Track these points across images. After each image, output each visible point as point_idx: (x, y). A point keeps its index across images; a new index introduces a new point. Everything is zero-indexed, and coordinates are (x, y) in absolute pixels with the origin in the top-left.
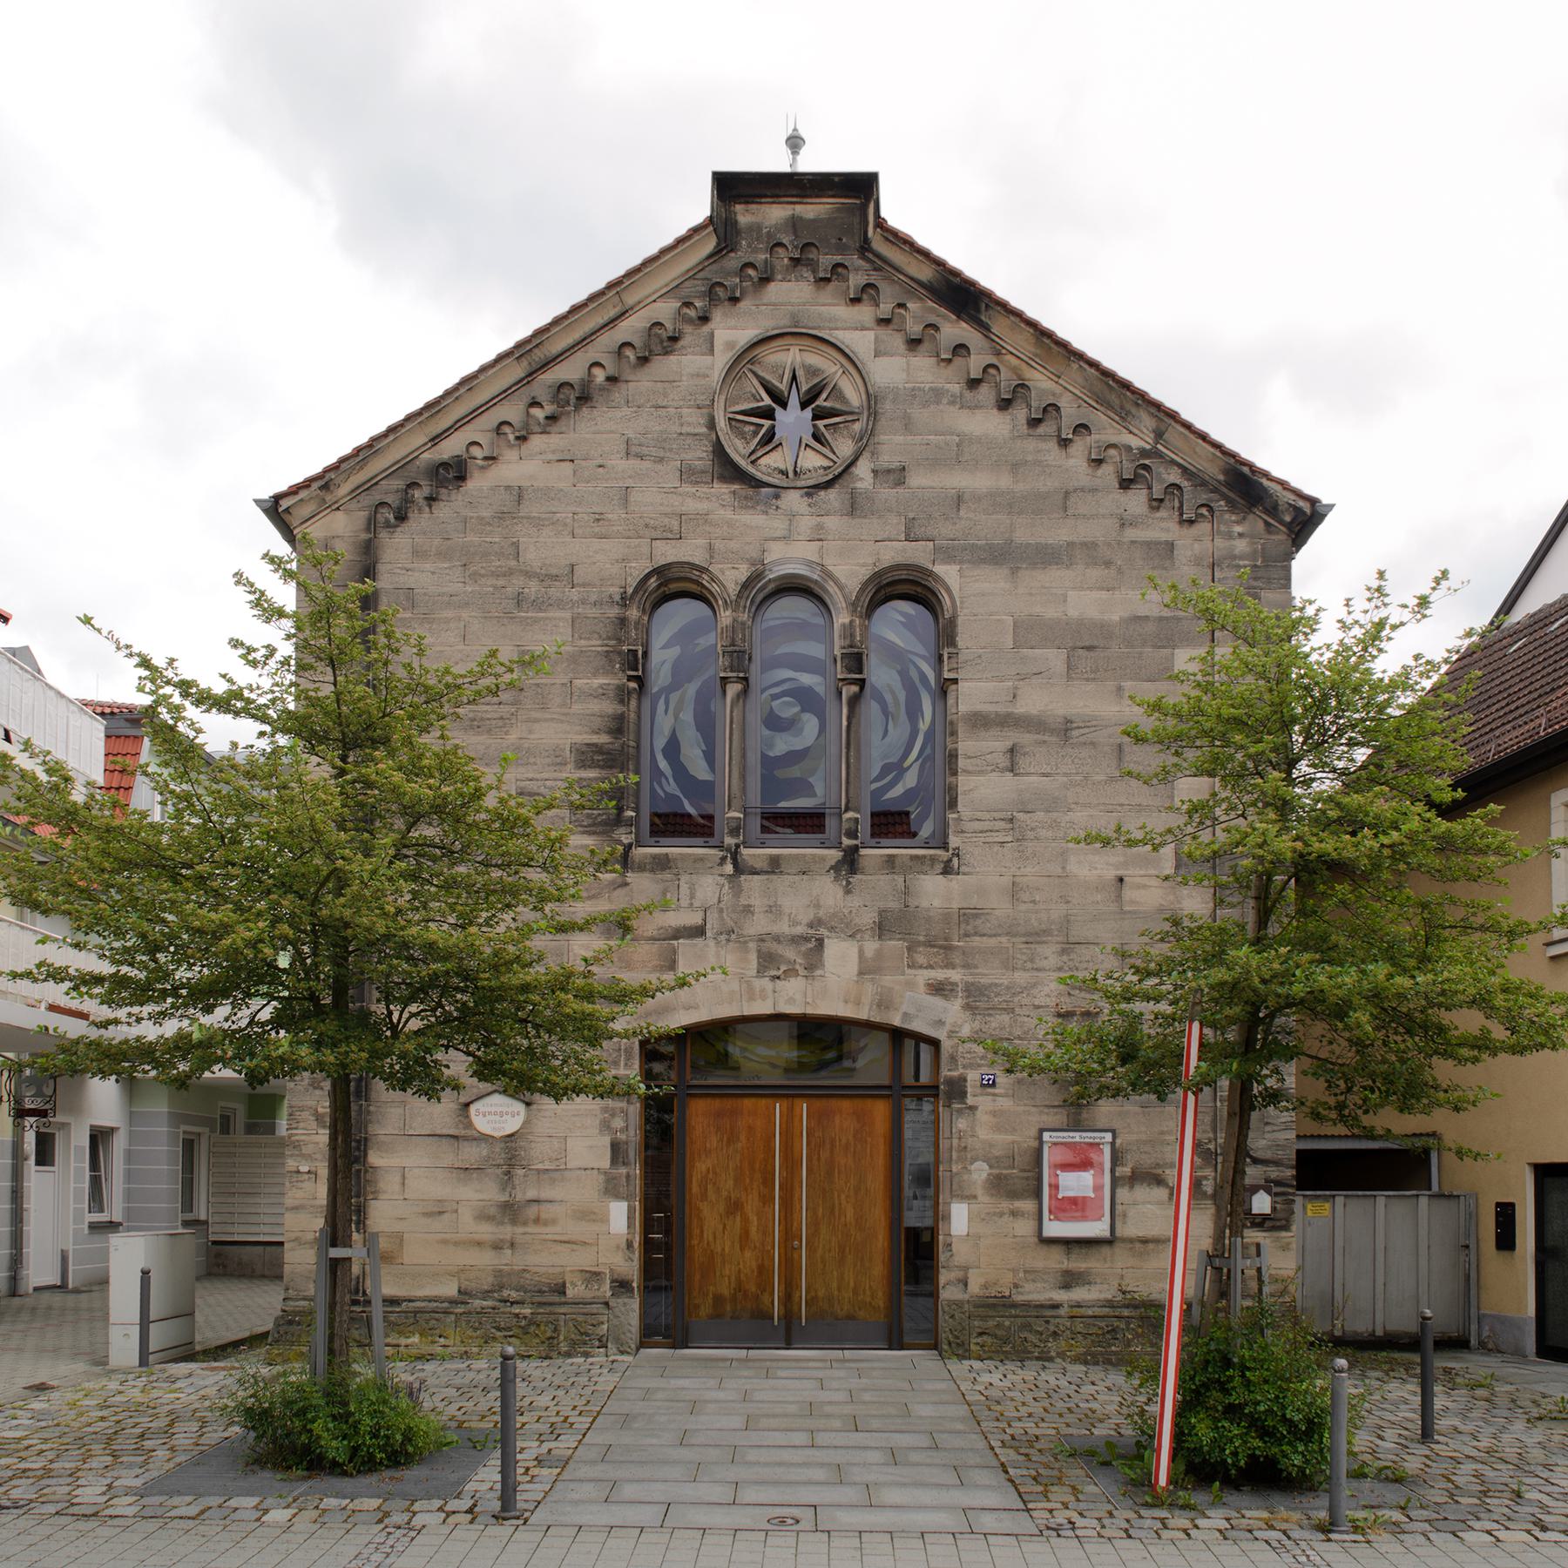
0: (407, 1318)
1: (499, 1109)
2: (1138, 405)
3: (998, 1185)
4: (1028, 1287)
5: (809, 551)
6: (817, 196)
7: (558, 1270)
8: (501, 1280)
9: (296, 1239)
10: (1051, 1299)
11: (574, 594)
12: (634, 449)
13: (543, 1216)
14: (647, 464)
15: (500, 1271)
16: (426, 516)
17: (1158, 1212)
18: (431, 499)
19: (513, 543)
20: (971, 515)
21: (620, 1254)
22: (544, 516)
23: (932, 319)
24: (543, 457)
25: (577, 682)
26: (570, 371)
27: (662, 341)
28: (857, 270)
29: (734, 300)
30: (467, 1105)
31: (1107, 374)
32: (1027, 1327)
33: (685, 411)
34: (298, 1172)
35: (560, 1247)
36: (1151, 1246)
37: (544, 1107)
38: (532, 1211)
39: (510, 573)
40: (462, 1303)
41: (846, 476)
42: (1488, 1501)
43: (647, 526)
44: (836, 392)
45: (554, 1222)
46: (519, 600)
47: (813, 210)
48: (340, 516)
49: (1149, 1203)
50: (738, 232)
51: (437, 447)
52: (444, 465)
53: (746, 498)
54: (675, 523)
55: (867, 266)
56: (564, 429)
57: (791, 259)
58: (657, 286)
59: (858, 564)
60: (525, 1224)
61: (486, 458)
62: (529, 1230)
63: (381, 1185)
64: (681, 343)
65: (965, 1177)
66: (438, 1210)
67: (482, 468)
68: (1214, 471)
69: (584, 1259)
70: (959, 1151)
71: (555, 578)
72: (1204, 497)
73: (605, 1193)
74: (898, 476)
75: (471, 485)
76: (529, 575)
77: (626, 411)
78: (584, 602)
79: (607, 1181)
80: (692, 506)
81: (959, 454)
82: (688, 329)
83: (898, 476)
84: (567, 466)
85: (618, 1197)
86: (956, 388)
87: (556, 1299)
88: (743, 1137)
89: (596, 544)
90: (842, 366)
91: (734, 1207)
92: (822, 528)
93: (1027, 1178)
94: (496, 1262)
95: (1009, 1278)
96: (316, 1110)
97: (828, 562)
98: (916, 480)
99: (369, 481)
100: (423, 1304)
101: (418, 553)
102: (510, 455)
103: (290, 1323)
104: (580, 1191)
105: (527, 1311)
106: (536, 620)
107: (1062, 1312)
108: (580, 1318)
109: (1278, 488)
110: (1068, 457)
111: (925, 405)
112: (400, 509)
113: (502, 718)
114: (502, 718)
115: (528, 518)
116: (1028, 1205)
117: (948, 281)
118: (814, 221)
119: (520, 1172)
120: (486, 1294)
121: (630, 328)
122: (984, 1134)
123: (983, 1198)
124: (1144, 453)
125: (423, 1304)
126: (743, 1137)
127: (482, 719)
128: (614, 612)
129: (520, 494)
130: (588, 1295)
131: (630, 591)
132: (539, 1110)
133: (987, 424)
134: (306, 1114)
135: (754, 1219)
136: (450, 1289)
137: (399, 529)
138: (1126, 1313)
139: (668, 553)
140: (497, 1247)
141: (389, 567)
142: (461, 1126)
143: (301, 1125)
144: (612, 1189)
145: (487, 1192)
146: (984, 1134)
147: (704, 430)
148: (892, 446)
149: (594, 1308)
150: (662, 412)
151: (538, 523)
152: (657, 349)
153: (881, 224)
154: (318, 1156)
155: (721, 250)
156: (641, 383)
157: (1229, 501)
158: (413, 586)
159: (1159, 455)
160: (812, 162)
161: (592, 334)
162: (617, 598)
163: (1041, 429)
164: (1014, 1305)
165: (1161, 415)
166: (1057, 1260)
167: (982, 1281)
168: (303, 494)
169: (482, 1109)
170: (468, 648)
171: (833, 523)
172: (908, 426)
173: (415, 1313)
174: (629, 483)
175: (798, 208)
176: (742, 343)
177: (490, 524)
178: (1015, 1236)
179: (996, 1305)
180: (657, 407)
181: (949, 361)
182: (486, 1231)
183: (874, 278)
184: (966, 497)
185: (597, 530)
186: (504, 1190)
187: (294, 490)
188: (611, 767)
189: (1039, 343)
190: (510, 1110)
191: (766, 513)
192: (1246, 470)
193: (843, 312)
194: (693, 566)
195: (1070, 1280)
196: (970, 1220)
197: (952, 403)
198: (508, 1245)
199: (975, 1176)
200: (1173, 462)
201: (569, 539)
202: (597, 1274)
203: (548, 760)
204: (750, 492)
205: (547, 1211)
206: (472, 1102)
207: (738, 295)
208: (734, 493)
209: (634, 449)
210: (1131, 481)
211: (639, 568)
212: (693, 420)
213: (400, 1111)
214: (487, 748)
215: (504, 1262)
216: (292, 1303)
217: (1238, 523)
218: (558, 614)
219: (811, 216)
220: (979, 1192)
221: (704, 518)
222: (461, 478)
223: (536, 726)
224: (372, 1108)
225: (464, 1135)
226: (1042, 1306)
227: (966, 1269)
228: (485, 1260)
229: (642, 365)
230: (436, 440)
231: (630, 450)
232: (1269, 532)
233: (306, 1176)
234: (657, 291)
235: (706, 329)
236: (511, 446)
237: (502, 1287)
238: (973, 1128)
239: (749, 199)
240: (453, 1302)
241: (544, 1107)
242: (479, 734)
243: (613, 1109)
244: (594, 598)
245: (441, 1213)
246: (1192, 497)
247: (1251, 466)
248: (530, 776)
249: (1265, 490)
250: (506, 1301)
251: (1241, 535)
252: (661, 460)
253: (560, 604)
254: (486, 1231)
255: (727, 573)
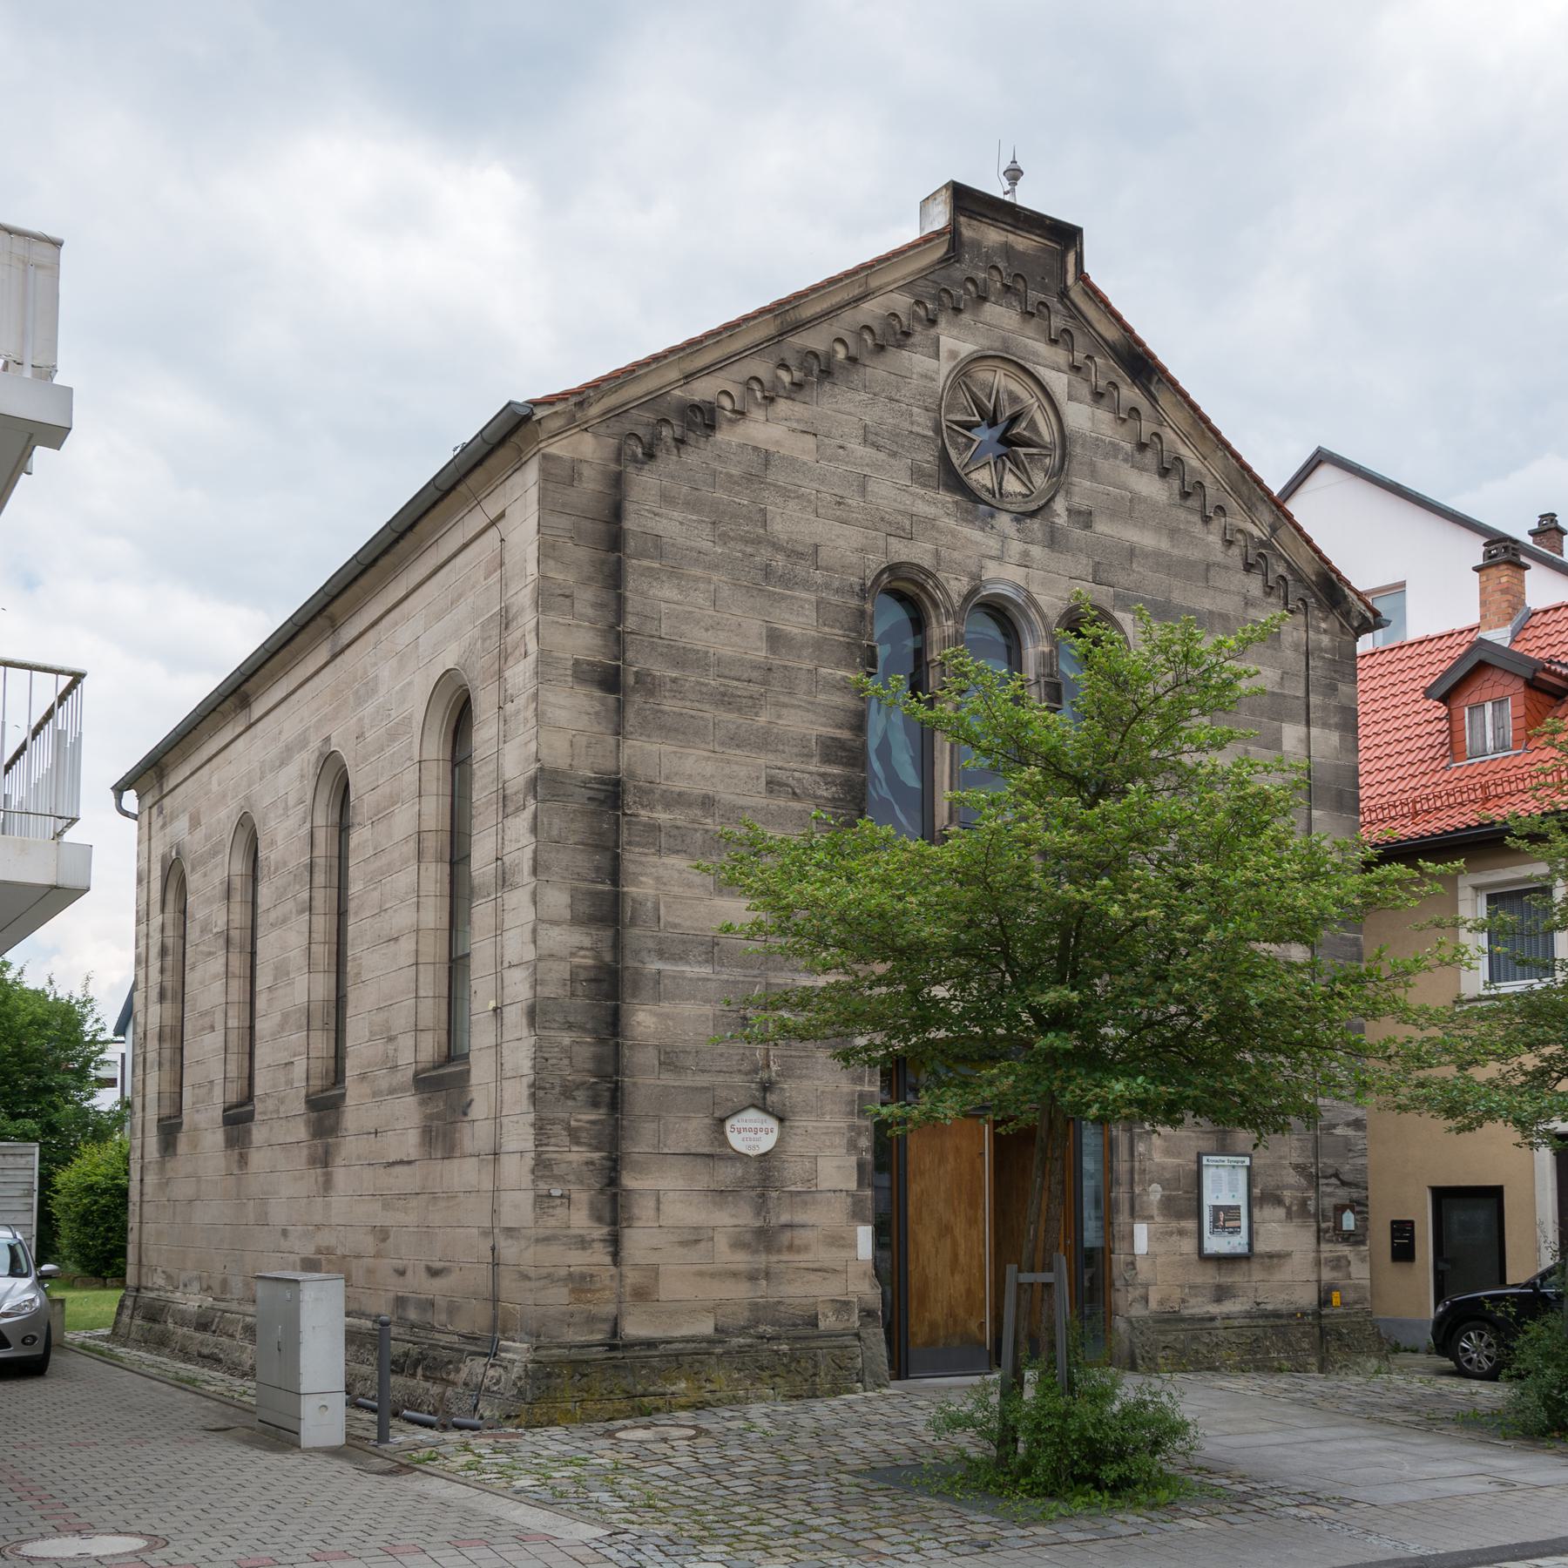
0: (668, 1362)
1: (753, 1125)
2: (1262, 499)
3: (1171, 1208)
4: (1192, 1301)
5: (1014, 574)
6: (1028, 232)
7: (811, 1300)
8: (758, 1312)
9: (548, 1276)
10: (1208, 1312)
11: (818, 576)
12: (871, 437)
13: (797, 1242)
14: (882, 456)
15: (756, 1304)
16: (675, 458)
17: (1279, 1230)
18: (680, 442)
19: (761, 510)
20: (1141, 570)
21: (867, 1281)
22: (790, 487)
23: (1114, 378)
24: (788, 424)
25: (823, 671)
26: (815, 340)
27: (893, 336)
28: (1057, 312)
29: (957, 310)
30: (722, 1121)
31: (1245, 468)
32: (1195, 1338)
33: (915, 410)
34: (550, 1196)
35: (812, 1276)
36: (1275, 1260)
37: (796, 1124)
38: (786, 1237)
39: (758, 541)
40: (720, 1342)
41: (1046, 510)
42: (752, 1489)
43: (882, 519)
44: (1033, 425)
45: (805, 1248)
46: (767, 571)
47: (1024, 243)
48: (588, 438)
49: (1273, 1221)
50: (962, 244)
51: (688, 386)
52: (695, 407)
53: (967, 511)
54: (907, 523)
55: (1064, 312)
56: (807, 399)
57: (1004, 285)
58: (897, 275)
59: (1056, 597)
60: (779, 1251)
61: (734, 411)
62: (784, 1257)
63: (636, 1211)
64: (912, 340)
65: (1145, 1198)
66: (694, 1238)
67: (730, 421)
68: (1309, 570)
69: (831, 1288)
70: (1140, 1174)
71: (801, 555)
72: (1302, 592)
73: (853, 1217)
74: (1084, 518)
75: (721, 436)
76: (777, 547)
77: (864, 396)
78: (827, 586)
79: (854, 1204)
80: (922, 508)
81: (1129, 509)
82: (918, 328)
83: (1084, 518)
84: (810, 438)
85: (864, 1221)
86: (1128, 447)
87: (809, 1331)
88: (951, 1159)
89: (838, 528)
90: (1038, 399)
91: (946, 1230)
92: (1028, 555)
93: (1189, 1199)
94: (750, 1295)
95: (1177, 1294)
96: (568, 1123)
97: (1033, 589)
98: (1102, 527)
99: (624, 405)
100: (681, 1346)
101: (666, 498)
102: (757, 414)
103: (549, 1375)
104: (826, 1216)
105: (785, 1347)
106: (783, 598)
107: (1217, 1323)
108: (837, 1352)
109: (1355, 597)
110: (1209, 532)
111: (1106, 456)
112: (651, 446)
113: (751, 697)
114: (751, 697)
115: (775, 486)
116: (1190, 1225)
117: (1130, 347)
118: (1023, 254)
119: (774, 1194)
120: (743, 1330)
121: (872, 310)
122: (1158, 1158)
123: (1158, 1219)
124: (1262, 544)
125: (681, 1346)
126: (951, 1159)
127: (733, 695)
128: (854, 602)
129: (767, 458)
130: (840, 1326)
131: (869, 583)
132: (791, 1127)
133: (1151, 487)
134: (557, 1128)
135: (961, 1241)
136: (706, 1327)
137: (646, 467)
138: (1261, 1322)
139: (903, 552)
140: (753, 1277)
141: (636, 506)
142: (716, 1143)
143: (553, 1141)
144: (857, 1215)
145: (740, 1218)
146: (1158, 1158)
147: (931, 434)
148: (1083, 489)
149: (848, 1341)
150: (895, 405)
151: (785, 493)
152: (892, 340)
153: (1082, 276)
154: (572, 1178)
155: (950, 259)
156: (877, 371)
157: (1318, 600)
158: (661, 533)
159: (1273, 548)
160: (1027, 197)
161: (839, 308)
162: (857, 589)
163: (1189, 503)
164: (1183, 1320)
165: (1280, 514)
166: (1209, 1276)
167: (1158, 1297)
168: (559, 407)
169: (738, 1125)
170: (719, 615)
171: (1036, 551)
172: (1093, 474)
173: (677, 1356)
174: (867, 471)
175: (1011, 237)
176: (962, 356)
177: (739, 485)
178: (1181, 1254)
179: (1170, 1319)
180: (891, 399)
181: (1124, 420)
182: (742, 1260)
183: (1070, 325)
184: (1137, 552)
185: (838, 513)
186: (758, 1214)
187: (549, 401)
188: (853, 765)
189: (1195, 424)
190: (764, 1126)
191: (983, 530)
192: (1334, 576)
193: (1042, 348)
194: (921, 569)
195: (1222, 1293)
196: (1149, 1239)
197: (1125, 460)
198: (763, 1275)
199: (1152, 1197)
200: (1281, 556)
201: (812, 517)
202: (846, 1303)
203: (795, 750)
204: (970, 505)
205: (802, 1236)
206: (728, 1117)
207: (962, 307)
208: (956, 503)
209: (871, 437)
210: (1252, 565)
211: (876, 562)
212: (921, 420)
213: (654, 1126)
214: (738, 727)
215: (759, 1294)
216: (544, 1352)
217: (1324, 620)
218: (804, 595)
219: (1020, 247)
220: (1155, 1212)
221: (931, 522)
222: (711, 427)
223: (784, 711)
224: (625, 1122)
225: (719, 1153)
226: (1202, 1319)
227: (1146, 1286)
228: (740, 1292)
229: (879, 352)
230: (689, 377)
231: (868, 437)
232: (1343, 633)
233: (558, 1202)
234: (895, 281)
235: (933, 332)
236: (759, 405)
237: (757, 1322)
238: (1149, 1151)
239: (972, 215)
240: (710, 1341)
241: (796, 1124)
242: (730, 711)
243: (859, 1127)
244: (836, 584)
245: (697, 1241)
246: (1295, 591)
247: (1338, 574)
248: (780, 764)
249: (1345, 597)
250: (762, 1338)
251: (1325, 631)
252: (894, 454)
253: (806, 585)
254: (742, 1260)
255: (952, 582)
